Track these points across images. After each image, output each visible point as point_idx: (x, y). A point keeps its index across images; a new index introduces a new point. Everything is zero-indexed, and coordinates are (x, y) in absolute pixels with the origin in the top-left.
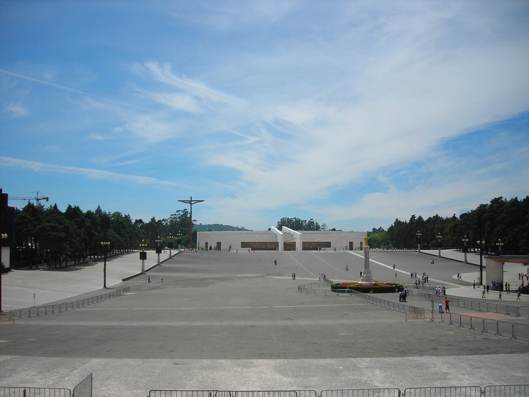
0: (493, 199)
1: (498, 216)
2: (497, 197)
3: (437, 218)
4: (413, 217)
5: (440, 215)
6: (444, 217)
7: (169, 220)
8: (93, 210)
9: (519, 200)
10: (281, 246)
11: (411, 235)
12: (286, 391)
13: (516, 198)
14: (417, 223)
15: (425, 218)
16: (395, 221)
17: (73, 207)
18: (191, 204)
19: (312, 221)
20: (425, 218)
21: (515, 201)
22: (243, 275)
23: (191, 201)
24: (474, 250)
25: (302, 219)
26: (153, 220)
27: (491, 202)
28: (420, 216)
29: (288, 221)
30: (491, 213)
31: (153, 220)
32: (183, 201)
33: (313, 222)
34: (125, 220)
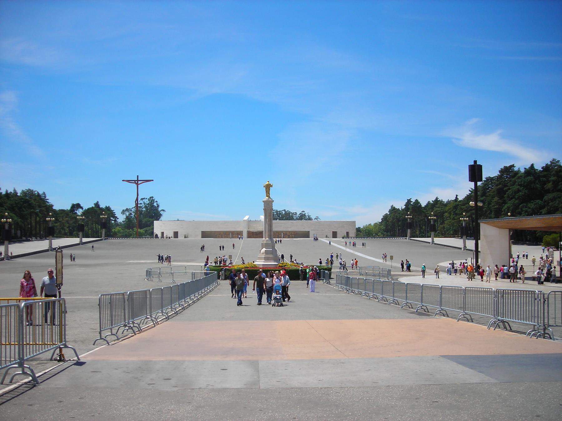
0: (502, 167)
1: (509, 189)
2: (508, 165)
3: (437, 202)
4: (409, 201)
5: (440, 199)
6: (445, 200)
7: (133, 210)
8: (11, 190)
9: (536, 167)
10: (245, 234)
11: (409, 222)
12: (533, 279)
13: (532, 165)
14: (413, 207)
15: (423, 204)
16: (390, 208)
17: (9, 192)
18: (137, 184)
19: (303, 213)
20: (423, 204)
21: (531, 171)
22: (139, 261)
23: (138, 180)
24: (476, 204)
25: (292, 211)
26: (97, 205)
27: (500, 172)
28: (417, 200)
29: (277, 214)
30: (500, 186)
31: (97, 205)
32: (128, 181)
33: (305, 215)
34: (31, 198)
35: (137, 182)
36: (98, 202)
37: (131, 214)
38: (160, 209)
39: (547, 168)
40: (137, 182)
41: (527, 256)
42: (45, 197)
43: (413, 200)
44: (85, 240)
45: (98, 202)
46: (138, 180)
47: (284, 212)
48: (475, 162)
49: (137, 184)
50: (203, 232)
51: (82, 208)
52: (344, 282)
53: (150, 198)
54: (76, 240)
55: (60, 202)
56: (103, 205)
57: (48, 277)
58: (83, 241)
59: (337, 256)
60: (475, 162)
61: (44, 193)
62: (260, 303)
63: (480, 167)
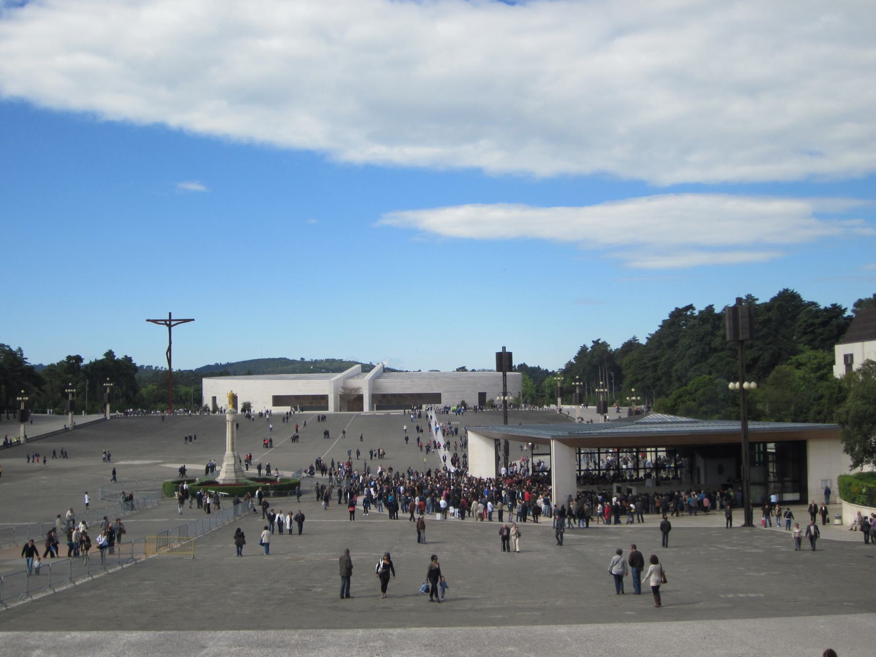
18: (170, 326)
20: (643, 341)
23: (170, 320)
26: (110, 354)
31: (110, 354)
32: (155, 321)
35: (169, 323)
39: (733, 311)
40: (169, 323)
42: (22, 355)
43: (589, 345)
46: (170, 320)
48: (504, 348)
49: (170, 326)
52: (130, 503)
56: (119, 355)
59: (358, 453)
60: (504, 348)
61: (20, 349)
62: (340, 503)
63: (510, 354)
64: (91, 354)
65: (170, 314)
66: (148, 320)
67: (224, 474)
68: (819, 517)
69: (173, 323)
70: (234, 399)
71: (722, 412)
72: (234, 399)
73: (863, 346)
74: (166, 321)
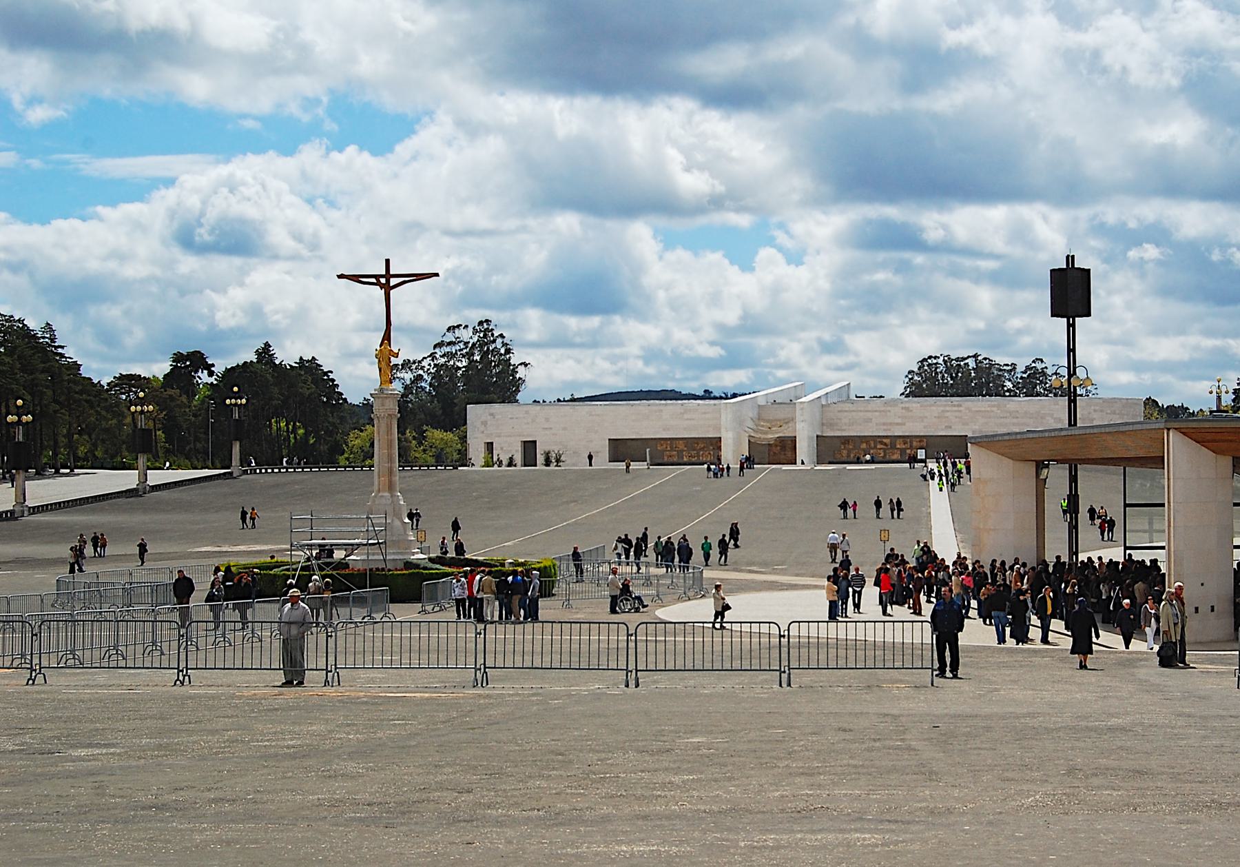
18: (387, 288)
19: (1039, 366)
23: (388, 276)
26: (265, 353)
31: (265, 353)
32: (356, 278)
35: (386, 282)
36: (267, 345)
37: (419, 378)
38: (515, 360)
40: (386, 282)
41: (897, 506)
42: (53, 340)
44: (156, 477)
45: (267, 345)
46: (388, 276)
47: (971, 363)
49: (387, 288)
50: (612, 441)
51: (209, 368)
53: (481, 323)
54: (127, 479)
55: (105, 351)
57: (963, 639)
58: (151, 482)
64: (241, 363)
65: (388, 261)
66: (341, 277)
67: (105, 830)
68: (850, 511)
69: (393, 281)
70: (1100, 558)
71: (1069, 538)
72: (1100, 558)
73: (1071, 326)
74: (377, 277)
